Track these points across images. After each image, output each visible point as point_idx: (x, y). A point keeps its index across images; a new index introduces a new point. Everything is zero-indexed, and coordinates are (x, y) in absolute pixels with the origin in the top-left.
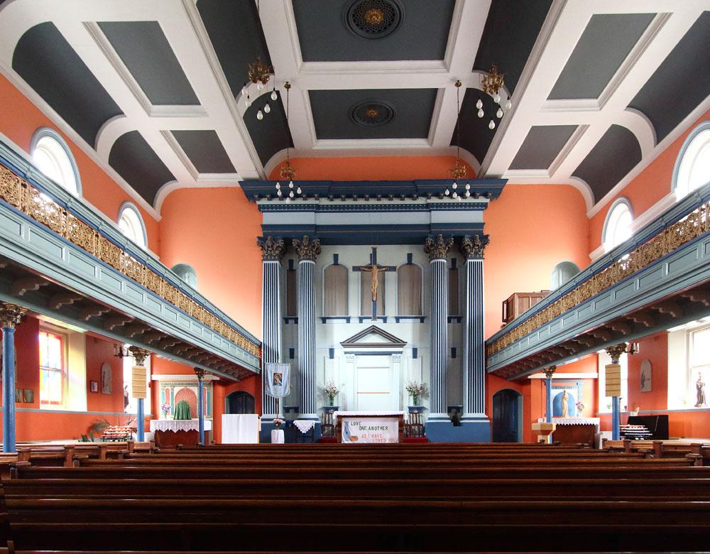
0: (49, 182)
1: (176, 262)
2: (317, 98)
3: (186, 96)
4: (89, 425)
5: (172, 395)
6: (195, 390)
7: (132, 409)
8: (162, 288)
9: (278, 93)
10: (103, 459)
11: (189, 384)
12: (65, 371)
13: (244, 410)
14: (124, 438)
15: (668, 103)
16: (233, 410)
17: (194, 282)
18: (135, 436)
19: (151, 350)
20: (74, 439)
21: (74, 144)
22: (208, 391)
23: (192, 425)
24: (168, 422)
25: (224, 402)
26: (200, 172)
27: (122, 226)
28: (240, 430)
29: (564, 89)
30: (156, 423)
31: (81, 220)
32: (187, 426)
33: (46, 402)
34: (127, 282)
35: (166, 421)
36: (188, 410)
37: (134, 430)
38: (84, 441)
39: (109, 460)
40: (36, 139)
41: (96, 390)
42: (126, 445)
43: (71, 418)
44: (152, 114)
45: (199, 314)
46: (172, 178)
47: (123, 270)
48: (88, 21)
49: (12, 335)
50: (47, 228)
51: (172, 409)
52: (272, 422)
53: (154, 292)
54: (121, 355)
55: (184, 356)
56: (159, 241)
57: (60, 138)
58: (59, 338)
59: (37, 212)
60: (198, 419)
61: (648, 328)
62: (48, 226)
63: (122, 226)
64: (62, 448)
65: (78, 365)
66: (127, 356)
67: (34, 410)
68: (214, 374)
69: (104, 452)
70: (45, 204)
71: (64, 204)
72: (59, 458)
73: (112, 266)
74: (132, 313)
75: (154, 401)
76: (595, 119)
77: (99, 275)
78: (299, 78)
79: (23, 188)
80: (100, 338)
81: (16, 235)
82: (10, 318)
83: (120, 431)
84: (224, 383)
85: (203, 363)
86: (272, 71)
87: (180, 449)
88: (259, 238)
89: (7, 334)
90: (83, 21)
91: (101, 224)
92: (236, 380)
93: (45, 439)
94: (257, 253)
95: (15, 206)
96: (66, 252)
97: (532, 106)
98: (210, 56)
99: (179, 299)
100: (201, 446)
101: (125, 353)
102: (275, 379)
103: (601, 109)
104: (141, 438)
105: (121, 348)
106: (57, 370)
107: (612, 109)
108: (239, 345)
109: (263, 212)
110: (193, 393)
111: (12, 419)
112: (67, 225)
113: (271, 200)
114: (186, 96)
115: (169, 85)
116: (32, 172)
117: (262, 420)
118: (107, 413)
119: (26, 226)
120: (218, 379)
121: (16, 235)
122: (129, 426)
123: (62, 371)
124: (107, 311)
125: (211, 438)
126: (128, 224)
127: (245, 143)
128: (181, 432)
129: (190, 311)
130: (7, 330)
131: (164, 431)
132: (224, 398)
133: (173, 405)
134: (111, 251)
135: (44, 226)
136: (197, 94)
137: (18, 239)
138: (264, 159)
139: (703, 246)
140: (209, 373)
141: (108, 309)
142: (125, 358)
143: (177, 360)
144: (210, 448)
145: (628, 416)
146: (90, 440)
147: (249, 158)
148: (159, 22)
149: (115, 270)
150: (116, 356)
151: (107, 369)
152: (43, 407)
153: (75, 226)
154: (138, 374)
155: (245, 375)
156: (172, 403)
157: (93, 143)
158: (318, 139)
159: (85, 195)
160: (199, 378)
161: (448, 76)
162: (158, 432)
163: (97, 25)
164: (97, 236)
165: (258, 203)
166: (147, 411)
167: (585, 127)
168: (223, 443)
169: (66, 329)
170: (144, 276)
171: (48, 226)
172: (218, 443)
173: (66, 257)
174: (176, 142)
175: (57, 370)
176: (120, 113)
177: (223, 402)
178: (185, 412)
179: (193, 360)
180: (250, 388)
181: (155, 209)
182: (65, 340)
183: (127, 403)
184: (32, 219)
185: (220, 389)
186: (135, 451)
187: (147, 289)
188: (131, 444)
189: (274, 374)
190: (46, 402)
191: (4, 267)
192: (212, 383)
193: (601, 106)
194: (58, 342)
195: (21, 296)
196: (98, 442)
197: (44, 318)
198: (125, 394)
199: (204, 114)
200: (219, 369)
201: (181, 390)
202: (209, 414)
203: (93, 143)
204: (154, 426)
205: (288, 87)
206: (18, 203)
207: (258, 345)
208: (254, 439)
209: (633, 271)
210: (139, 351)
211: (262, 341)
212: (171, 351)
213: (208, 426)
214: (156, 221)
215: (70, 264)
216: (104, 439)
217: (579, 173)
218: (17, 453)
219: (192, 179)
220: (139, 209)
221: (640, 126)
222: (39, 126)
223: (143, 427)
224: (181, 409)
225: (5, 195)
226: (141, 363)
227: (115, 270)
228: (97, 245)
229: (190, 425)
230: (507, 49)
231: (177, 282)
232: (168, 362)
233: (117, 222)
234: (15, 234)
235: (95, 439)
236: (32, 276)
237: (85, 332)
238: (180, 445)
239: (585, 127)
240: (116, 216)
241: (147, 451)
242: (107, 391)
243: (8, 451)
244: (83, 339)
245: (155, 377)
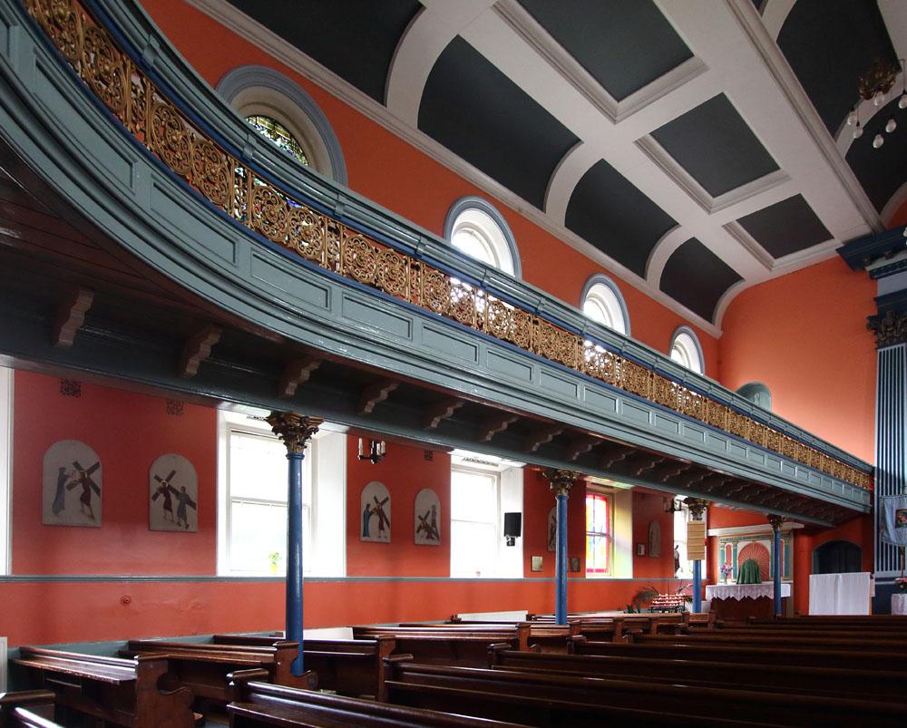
0: (597, 328)
1: (742, 383)
4: (635, 593)
5: (735, 555)
6: (768, 544)
7: (685, 571)
8: (728, 420)
10: (654, 634)
11: (758, 537)
12: (611, 534)
14: (676, 609)
16: (824, 569)
17: (774, 404)
18: (690, 607)
19: (709, 499)
20: (619, 610)
21: (623, 281)
22: (787, 545)
23: (764, 590)
24: (729, 587)
25: (810, 558)
27: (675, 356)
28: (840, 596)
30: (712, 590)
31: (634, 362)
32: (755, 592)
33: (591, 571)
34: (685, 422)
35: (726, 585)
36: (757, 571)
37: (688, 599)
38: (629, 612)
39: (661, 635)
41: (643, 553)
42: (680, 617)
43: (615, 588)
44: (617, 119)
45: (777, 443)
46: (736, 278)
47: (680, 409)
48: (640, 137)
49: (565, 502)
50: (453, 323)
51: (735, 571)
52: (893, 583)
53: (668, 406)
54: (673, 510)
55: (753, 501)
56: (719, 362)
57: (610, 280)
58: (606, 499)
59: (592, 368)
60: (773, 583)
62: (602, 379)
63: (675, 356)
64: (611, 621)
65: (624, 531)
66: (680, 510)
67: (579, 579)
68: (795, 521)
69: (654, 626)
70: (592, 353)
71: (412, 252)
72: (607, 631)
73: (666, 407)
74: (685, 456)
75: (711, 560)
77: (652, 419)
79: (415, 271)
80: (647, 492)
81: (526, 381)
82: (563, 486)
83: (671, 600)
84: (810, 531)
85: (781, 509)
87: (752, 623)
88: (871, 318)
89: (561, 502)
91: (686, 376)
92: (830, 526)
93: (590, 612)
94: (867, 340)
95: (470, 325)
96: (653, 416)
98: (811, 121)
99: (748, 429)
100: (779, 618)
101: (677, 506)
102: (898, 519)
104: (697, 608)
105: (673, 502)
106: (602, 535)
108: (836, 477)
109: (877, 279)
110: (763, 548)
111: (564, 590)
112: (619, 372)
113: (891, 257)
114: (757, 163)
116: (343, 204)
117: (877, 580)
118: (655, 579)
119: (582, 385)
120: (802, 526)
121: (526, 381)
122: (681, 594)
123: (607, 535)
124: (661, 461)
125: (790, 606)
126: (681, 353)
127: (844, 184)
128: (747, 600)
130: (561, 498)
131: (755, 598)
132: (809, 553)
133: (735, 565)
134: (636, 376)
135: (598, 380)
136: (748, 123)
137: (575, 402)
138: (879, 204)
140: (789, 520)
141: (662, 457)
142: (677, 514)
143: (742, 507)
144: (792, 622)
145: (527, 635)
146: (636, 610)
147: (855, 210)
150: (667, 511)
151: (655, 528)
152: (589, 576)
153: (497, 312)
154: (692, 530)
155: (841, 515)
156: (735, 563)
157: (541, 204)
159: (707, 374)
160: (775, 527)
162: (716, 601)
163: (737, 224)
164: (652, 376)
165: (869, 268)
166: (704, 576)
168: (810, 614)
169: (612, 487)
170: (706, 410)
171: (602, 379)
172: (801, 612)
173: (619, 408)
174: (760, 247)
175: (602, 535)
176: (575, 141)
177: (808, 556)
178: (751, 573)
179: (767, 505)
180: (853, 536)
182: (611, 500)
183: (677, 566)
184: (350, 282)
185: (805, 541)
186: (691, 624)
188: (686, 615)
189: (897, 511)
190: (591, 571)
191: (394, 388)
192: (792, 534)
194: (604, 503)
195: (434, 428)
196: (644, 614)
197: (592, 479)
198: (675, 555)
199: (786, 178)
200: (805, 514)
201: (767, 552)
202: (787, 575)
204: (709, 593)
206: (575, 364)
207: (865, 471)
208: (864, 609)
210: (696, 502)
211: (876, 465)
212: (736, 498)
213: (786, 590)
214: (714, 339)
215: (624, 415)
216: (652, 610)
218: (568, 626)
219: (766, 270)
220: (614, 281)
222: (459, 193)
223: (700, 595)
224: (747, 570)
225: (456, 315)
226: (699, 517)
227: (670, 410)
228: (650, 387)
229: (759, 591)
231: (747, 408)
232: (726, 510)
233: (669, 353)
235: (642, 610)
236: (448, 396)
237: (632, 488)
238: (751, 617)
240: (668, 345)
241: (705, 625)
242: (655, 553)
243: (561, 624)
244: (629, 498)
245: (713, 532)
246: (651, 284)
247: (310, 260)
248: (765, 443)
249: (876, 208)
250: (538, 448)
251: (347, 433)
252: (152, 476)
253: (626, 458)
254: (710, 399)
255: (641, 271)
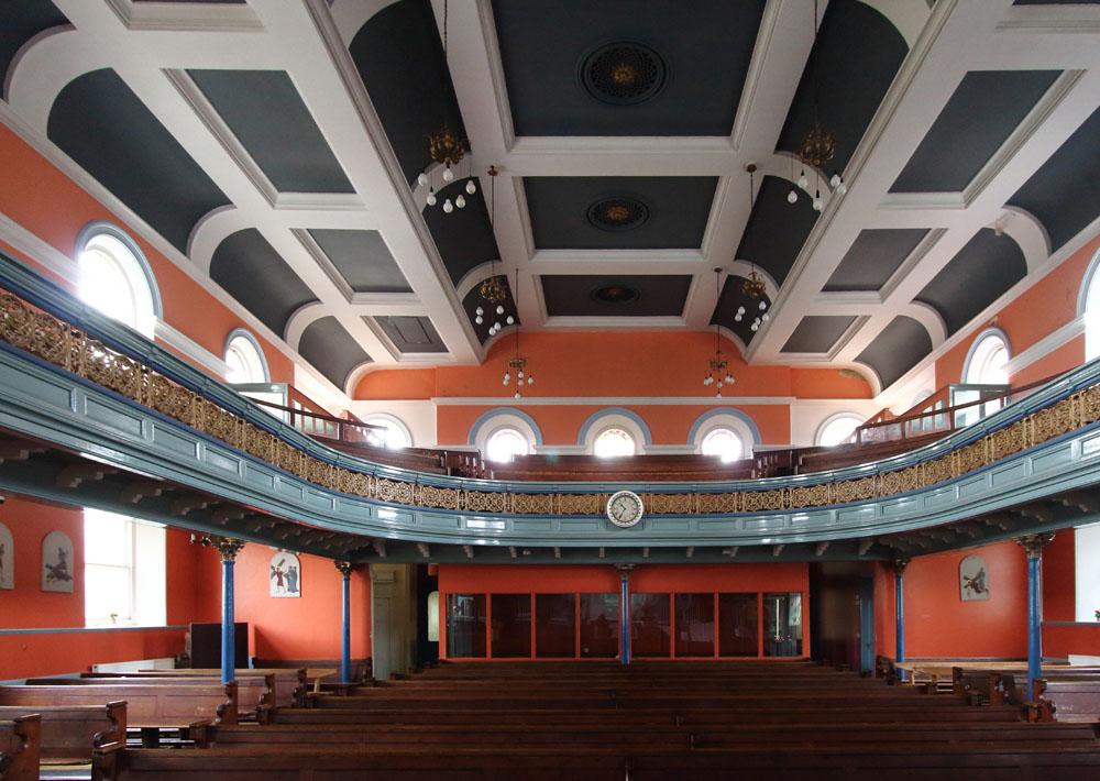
2: (533, 187)
3: (334, 181)
9: (476, 181)
13: (62, 586)
15: (1076, 194)
26: (280, 190)
29: (912, 180)
40: (84, 238)
48: (171, 67)
53: (261, 457)
61: (1041, 523)
76: (953, 223)
78: (513, 159)
86: (468, 149)
90: (162, 67)
96: (201, 449)
97: (860, 201)
103: (966, 207)
107: (986, 205)
114: (334, 181)
115: (303, 165)
124: (216, 502)
129: (304, 475)
139: (990, 476)
148: (289, 72)
149: (227, 445)
158: (517, 135)
161: (729, 159)
163: (185, 74)
164: (303, 456)
167: (941, 232)
181: (189, 258)
187: (280, 470)
193: (968, 202)
203: (182, 244)
205: (493, 173)
206: (193, 421)
209: (983, 464)
217: (1021, 200)
221: (1026, 232)
230: (832, 110)
234: (189, 456)
239: (941, 232)
246: (196, 265)
247: (54, 363)
248: (304, 475)
249: (479, 338)
250: (227, 523)
251: (166, 528)
252: (44, 564)
253: (163, 494)
254: (282, 440)
255: (182, 244)
